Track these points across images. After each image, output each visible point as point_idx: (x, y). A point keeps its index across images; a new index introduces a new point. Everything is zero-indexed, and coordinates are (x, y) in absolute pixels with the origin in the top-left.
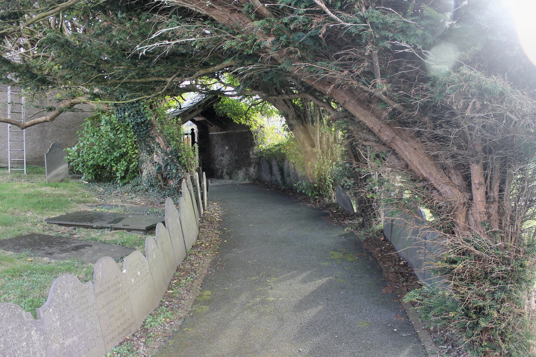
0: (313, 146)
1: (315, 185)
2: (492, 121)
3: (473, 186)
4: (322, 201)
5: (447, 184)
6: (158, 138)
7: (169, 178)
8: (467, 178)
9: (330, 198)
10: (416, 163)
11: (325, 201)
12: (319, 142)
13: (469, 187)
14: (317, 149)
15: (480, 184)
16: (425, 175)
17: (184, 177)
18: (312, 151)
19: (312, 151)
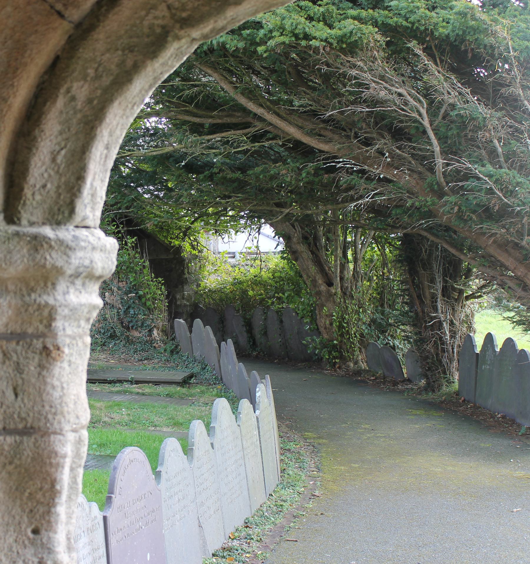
0: (330, 284)
1: (335, 342)
4: (344, 366)
7: (132, 327)
9: (356, 363)
11: (349, 366)
12: (339, 278)
14: (337, 289)
17: (155, 326)
19: (328, 291)
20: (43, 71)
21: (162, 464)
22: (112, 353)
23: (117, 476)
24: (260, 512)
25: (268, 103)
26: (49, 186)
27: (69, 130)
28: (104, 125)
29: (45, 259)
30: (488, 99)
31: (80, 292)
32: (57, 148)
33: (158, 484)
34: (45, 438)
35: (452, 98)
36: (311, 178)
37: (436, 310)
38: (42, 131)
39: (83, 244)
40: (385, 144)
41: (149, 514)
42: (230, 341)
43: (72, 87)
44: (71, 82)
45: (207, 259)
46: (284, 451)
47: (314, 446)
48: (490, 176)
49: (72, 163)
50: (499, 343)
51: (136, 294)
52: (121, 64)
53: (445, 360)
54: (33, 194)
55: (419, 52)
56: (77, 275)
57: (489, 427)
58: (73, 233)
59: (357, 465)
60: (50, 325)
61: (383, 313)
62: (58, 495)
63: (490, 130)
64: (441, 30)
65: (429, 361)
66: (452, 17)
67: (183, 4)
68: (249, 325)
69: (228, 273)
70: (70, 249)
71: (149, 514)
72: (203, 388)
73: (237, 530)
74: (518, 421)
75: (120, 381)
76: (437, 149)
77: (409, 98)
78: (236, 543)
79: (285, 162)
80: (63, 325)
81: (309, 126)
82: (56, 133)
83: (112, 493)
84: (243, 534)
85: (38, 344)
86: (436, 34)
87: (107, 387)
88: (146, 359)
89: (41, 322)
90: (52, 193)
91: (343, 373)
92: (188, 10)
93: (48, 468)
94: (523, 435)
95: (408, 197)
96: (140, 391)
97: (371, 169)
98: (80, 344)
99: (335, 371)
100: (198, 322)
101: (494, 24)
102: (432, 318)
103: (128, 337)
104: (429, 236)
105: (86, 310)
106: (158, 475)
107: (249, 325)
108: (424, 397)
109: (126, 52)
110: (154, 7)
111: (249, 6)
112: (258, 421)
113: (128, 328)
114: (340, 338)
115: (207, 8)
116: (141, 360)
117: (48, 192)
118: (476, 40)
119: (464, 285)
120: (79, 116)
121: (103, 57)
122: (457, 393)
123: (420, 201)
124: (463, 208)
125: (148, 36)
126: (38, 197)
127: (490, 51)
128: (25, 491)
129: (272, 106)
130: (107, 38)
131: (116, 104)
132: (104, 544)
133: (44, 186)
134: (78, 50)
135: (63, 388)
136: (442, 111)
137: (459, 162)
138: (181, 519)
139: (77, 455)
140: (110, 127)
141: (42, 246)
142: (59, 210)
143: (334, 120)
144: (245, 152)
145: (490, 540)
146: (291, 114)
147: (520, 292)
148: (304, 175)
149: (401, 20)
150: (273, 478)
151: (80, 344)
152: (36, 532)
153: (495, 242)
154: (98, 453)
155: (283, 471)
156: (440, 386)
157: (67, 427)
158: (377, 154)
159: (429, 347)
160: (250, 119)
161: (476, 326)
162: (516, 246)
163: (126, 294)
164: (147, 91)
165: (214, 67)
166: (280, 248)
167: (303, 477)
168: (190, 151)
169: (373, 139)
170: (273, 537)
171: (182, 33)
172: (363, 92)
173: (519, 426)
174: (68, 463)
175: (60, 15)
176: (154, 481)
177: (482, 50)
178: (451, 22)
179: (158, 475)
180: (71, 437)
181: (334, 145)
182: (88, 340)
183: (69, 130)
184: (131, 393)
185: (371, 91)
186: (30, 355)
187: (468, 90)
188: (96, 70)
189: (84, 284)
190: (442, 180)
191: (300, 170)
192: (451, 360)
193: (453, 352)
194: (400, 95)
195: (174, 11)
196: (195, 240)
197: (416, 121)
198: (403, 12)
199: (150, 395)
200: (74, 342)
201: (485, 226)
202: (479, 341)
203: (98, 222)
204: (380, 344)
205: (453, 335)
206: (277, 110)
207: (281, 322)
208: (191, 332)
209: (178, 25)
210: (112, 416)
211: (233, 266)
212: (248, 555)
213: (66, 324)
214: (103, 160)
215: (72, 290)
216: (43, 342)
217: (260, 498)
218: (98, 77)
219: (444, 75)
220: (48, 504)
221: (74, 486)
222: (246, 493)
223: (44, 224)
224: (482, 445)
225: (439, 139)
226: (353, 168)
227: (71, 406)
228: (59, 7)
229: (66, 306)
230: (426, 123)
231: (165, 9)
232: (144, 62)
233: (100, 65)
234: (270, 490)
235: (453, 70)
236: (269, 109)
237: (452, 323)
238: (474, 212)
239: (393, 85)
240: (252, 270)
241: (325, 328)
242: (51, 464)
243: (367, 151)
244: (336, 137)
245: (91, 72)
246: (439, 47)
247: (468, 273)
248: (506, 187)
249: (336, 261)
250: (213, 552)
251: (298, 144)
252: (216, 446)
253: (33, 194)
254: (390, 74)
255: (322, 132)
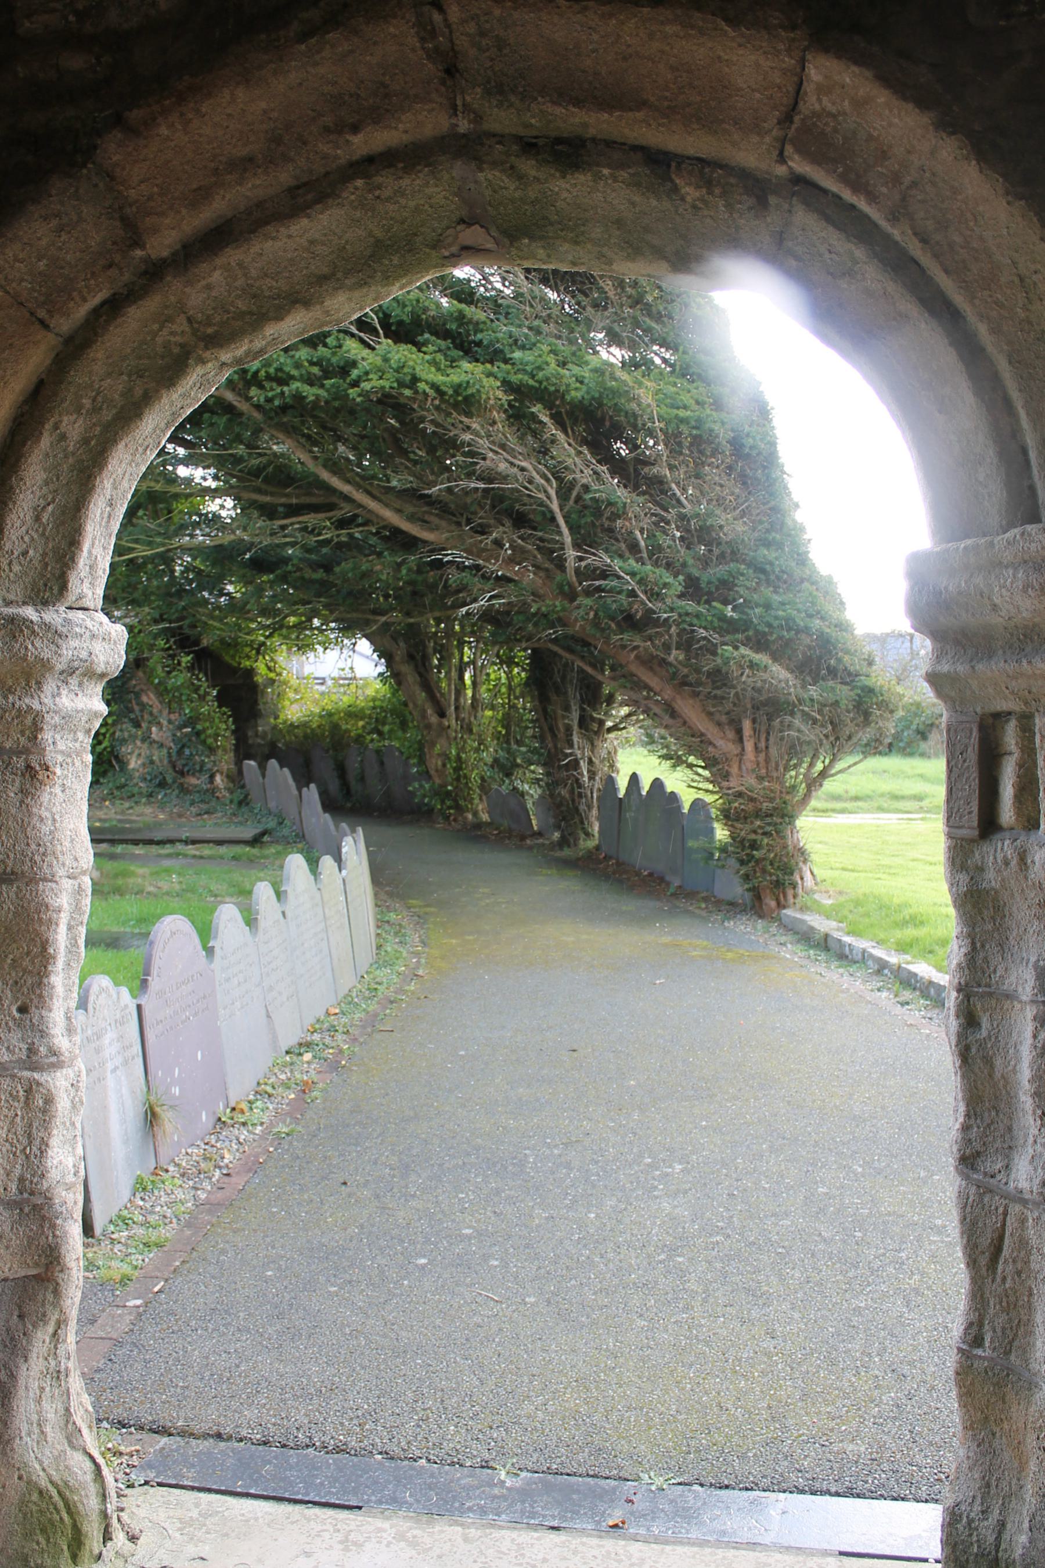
0: (442, 714)
1: (449, 788)
2: (759, 684)
3: (745, 738)
5: (722, 738)
6: (148, 696)
7: (188, 771)
8: (739, 732)
9: (475, 814)
10: (695, 720)
11: (466, 818)
12: (453, 708)
13: (741, 740)
15: (750, 736)
16: (703, 731)
17: (218, 771)
18: (440, 724)
19: (440, 724)
20: (21, 398)
21: (216, 937)
22: (162, 806)
23: (154, 953)
24: (348, 999)
25: (357, 479)
26: (31, 552)
27: (58, 479)
28: (105, 473)
29: (26, 648)
30: (629, 481)
31: (77, 695)
32: (42, 502)
33: (212, 961)
34: (32, 886)
35: (585, 477)
36: (414, 576)
37: (571, 746)
38: (22, 479)
39: (78, 630)
40: (505, 533)
41: (198, 1001)
42: (312, 786)
43: (61, 422)
44: (60, 415)
45: (285, 683)
46: (380, 923)
47: (419, 916)
48: (633, 574)
49: (63, 523)
50: (646, 786)
51: (193, 728)
52: (128, 392)
53: (582, 807)
54: (10, 564)
55: (545, 419)
56: (71, 671)
57: (631, 888)
58: (64, 615)
59: (471, 938)
60: (36, 738)
61: (508, 751)
62: (51, 961)
63: (631, 519)
64: (573, 393)
65: (564, 808)
66: (587, 375)
67: (208, 317)
68: (341, 770)
69: (316, 702)
70: (60, 636)
71: (198, 1001)
72: (280, 848)
73: (318, 1021)
74: (667, 878)
75: (172, 842)
76: (568, 539)
77: (534, 474)
78: (316, 1037)
79: (379, 555)
80: (53, 737)
81: (410, 509)
82: (40, 482)
83: (148, 975)
84: (326, 1025)
85: (20, 763)
86: (568, 398)
87: (154, 849)
88: (206, 813)
89: (23, 733)
90: (36, 562)
91: (459, 827)
92: (214, 325)
93: (37, 926)
94: (672, 895)
95: (533, 601)
96: (197, 853)
97: (487, 564)
98: (78, 763)
99: (450, 824)
100: (273, 763)
101: (636, 386)
102: (567, 756)
103: (182, 784)
104: (560, 651)
105: (84, 719)
106: (210, 951)
107: (341, 770)
108: (558, 854)
109: (134, 377)
110: (170, 319)
111: (293, 323)
112: (344, 884)
113: (182, 774)
114: (455, 783)
115: (240, 323)
116: (200, 815)
117: (31, 560)
118: (616, 404)
119: (606, 714)
120: (71, 460)
121: (102, 383)
122: (598, 848)
123: (547, 606)
124: (601, 614)
125: (163, 357)
126: (16, 568)
127: (632, 420)
128: (6, 956)
129: (362, 482)
130: (107, 358)
131: (121, 446)
132: (139, 1040)
133: (25, 553)
134: (68, 372)
135: (54, 820)
136: (574, 494)
137: (594, 555)
138: (242, 1008)
139: (77, 908)
140: (114, 476)
141: (22, 631)
142: (46, 585)
143: (440, 502)
144: (327, 542)
145: (627, 1018)
146: (386, 493)
147: (667, 719)
148: (404, 572)
149: (526, 378)
150: (366, 956)
151: (78, 763)
152: (23, 1010)
153: (637, 657)
154: (137, 931)
155: (379, 947)
156: (576, 840)
157: (61, 872)
158: (494, 546)
159: (564, 792)
160: (334, 499)
161: (618, 765)
162: (663, 662)
163: (180, 728)
164: (164, 432)
165: (290, 431)
166: (382, 669)
167: (405, 954)
168: (257, 540)
169: (489, 526)
170: (364, 1027)
171: (207, 354)
172: (477, 463)
173: (668, 884)
174: (64, 919)
175: (44, 324)
176: (204, 959)
177: (622, 418)
178: (586, 381)
179: (210, 951)
180: (67, 884)
181: (442, 533)
182: (89, 758)
183: (58, 479)
184: (185, 856)
185: (488, 462)
186: (9, 777)
187: (605, 468)
188: (94, 400)
189: (80, 684)
190: (574, 579)
191: (399, 565)
192: (590, 807)
193: (592, 797)
194: (523, 469)
195: (196, 326)
196: (272, 660)
197: (542, 504)
198: (529, 368)
199: (210, 858)
200: (69, 760)
201: (625, 636)
202: (622, 783)
203: (100, 603)
204: (504, 789)
205: (592, 775)
206: (369, 488)
207: (382, 763)
208: (264, 776)
209: (202, 344)
210: (159, 885)
211: (322, 694)
212: (331, 1051)
213: (58, 737)
214: (105, 520)
215: (64, 692)
216: (26, 760)
217: (348, 981)
218: (96, 410)
219: (575, 449)
220: (39, 974)
221: (74, 949)
222: (329, 974)
223: (25, 603)
224: (624, 908)
225: (570, 529)
226: (464, 562)
227: (67, 844)
228: (42, 313)
229: (55, 712)
230: (555, 506)
231: (185, 322)
232: (157, 391)
233: (98, 394)
234: (362, 971)
235: (584, 442)
236: (358, 486)
237: (590, 762)
238: (613, 619)
239: (515, 457)
240: (345, 699)
241: (437, 771)
242: (40, 919)
243: (481, 542)
244: (444, 523)
245: (87, 402)
246: (571, 414)
247: (610, 700)
248: (652, 589)
249: (449, 685)
250: (287, 1048)
251: (396, 531)
252: (288, 914)
253: (10, 564)
254: (512, 441)
255: (426, 517)
